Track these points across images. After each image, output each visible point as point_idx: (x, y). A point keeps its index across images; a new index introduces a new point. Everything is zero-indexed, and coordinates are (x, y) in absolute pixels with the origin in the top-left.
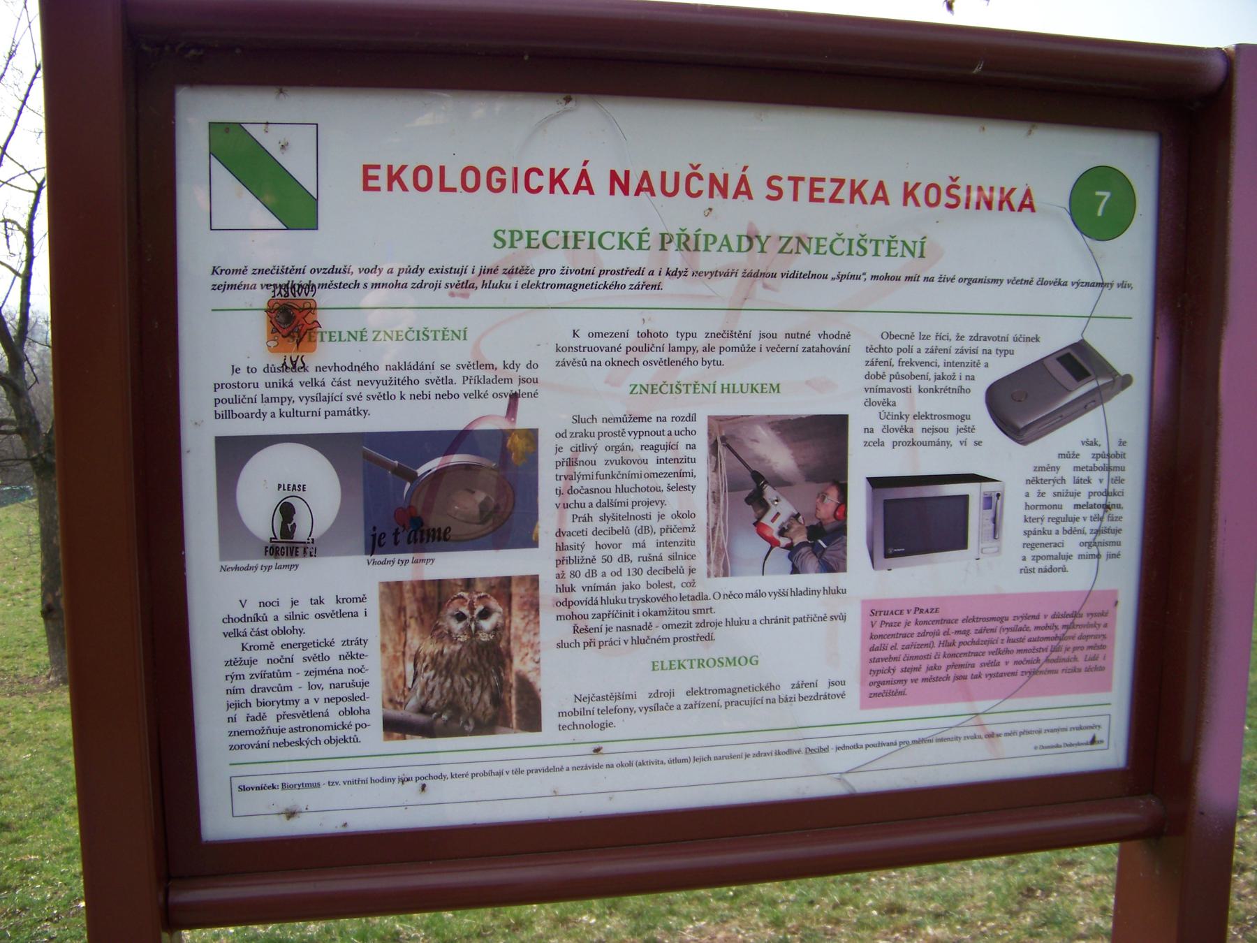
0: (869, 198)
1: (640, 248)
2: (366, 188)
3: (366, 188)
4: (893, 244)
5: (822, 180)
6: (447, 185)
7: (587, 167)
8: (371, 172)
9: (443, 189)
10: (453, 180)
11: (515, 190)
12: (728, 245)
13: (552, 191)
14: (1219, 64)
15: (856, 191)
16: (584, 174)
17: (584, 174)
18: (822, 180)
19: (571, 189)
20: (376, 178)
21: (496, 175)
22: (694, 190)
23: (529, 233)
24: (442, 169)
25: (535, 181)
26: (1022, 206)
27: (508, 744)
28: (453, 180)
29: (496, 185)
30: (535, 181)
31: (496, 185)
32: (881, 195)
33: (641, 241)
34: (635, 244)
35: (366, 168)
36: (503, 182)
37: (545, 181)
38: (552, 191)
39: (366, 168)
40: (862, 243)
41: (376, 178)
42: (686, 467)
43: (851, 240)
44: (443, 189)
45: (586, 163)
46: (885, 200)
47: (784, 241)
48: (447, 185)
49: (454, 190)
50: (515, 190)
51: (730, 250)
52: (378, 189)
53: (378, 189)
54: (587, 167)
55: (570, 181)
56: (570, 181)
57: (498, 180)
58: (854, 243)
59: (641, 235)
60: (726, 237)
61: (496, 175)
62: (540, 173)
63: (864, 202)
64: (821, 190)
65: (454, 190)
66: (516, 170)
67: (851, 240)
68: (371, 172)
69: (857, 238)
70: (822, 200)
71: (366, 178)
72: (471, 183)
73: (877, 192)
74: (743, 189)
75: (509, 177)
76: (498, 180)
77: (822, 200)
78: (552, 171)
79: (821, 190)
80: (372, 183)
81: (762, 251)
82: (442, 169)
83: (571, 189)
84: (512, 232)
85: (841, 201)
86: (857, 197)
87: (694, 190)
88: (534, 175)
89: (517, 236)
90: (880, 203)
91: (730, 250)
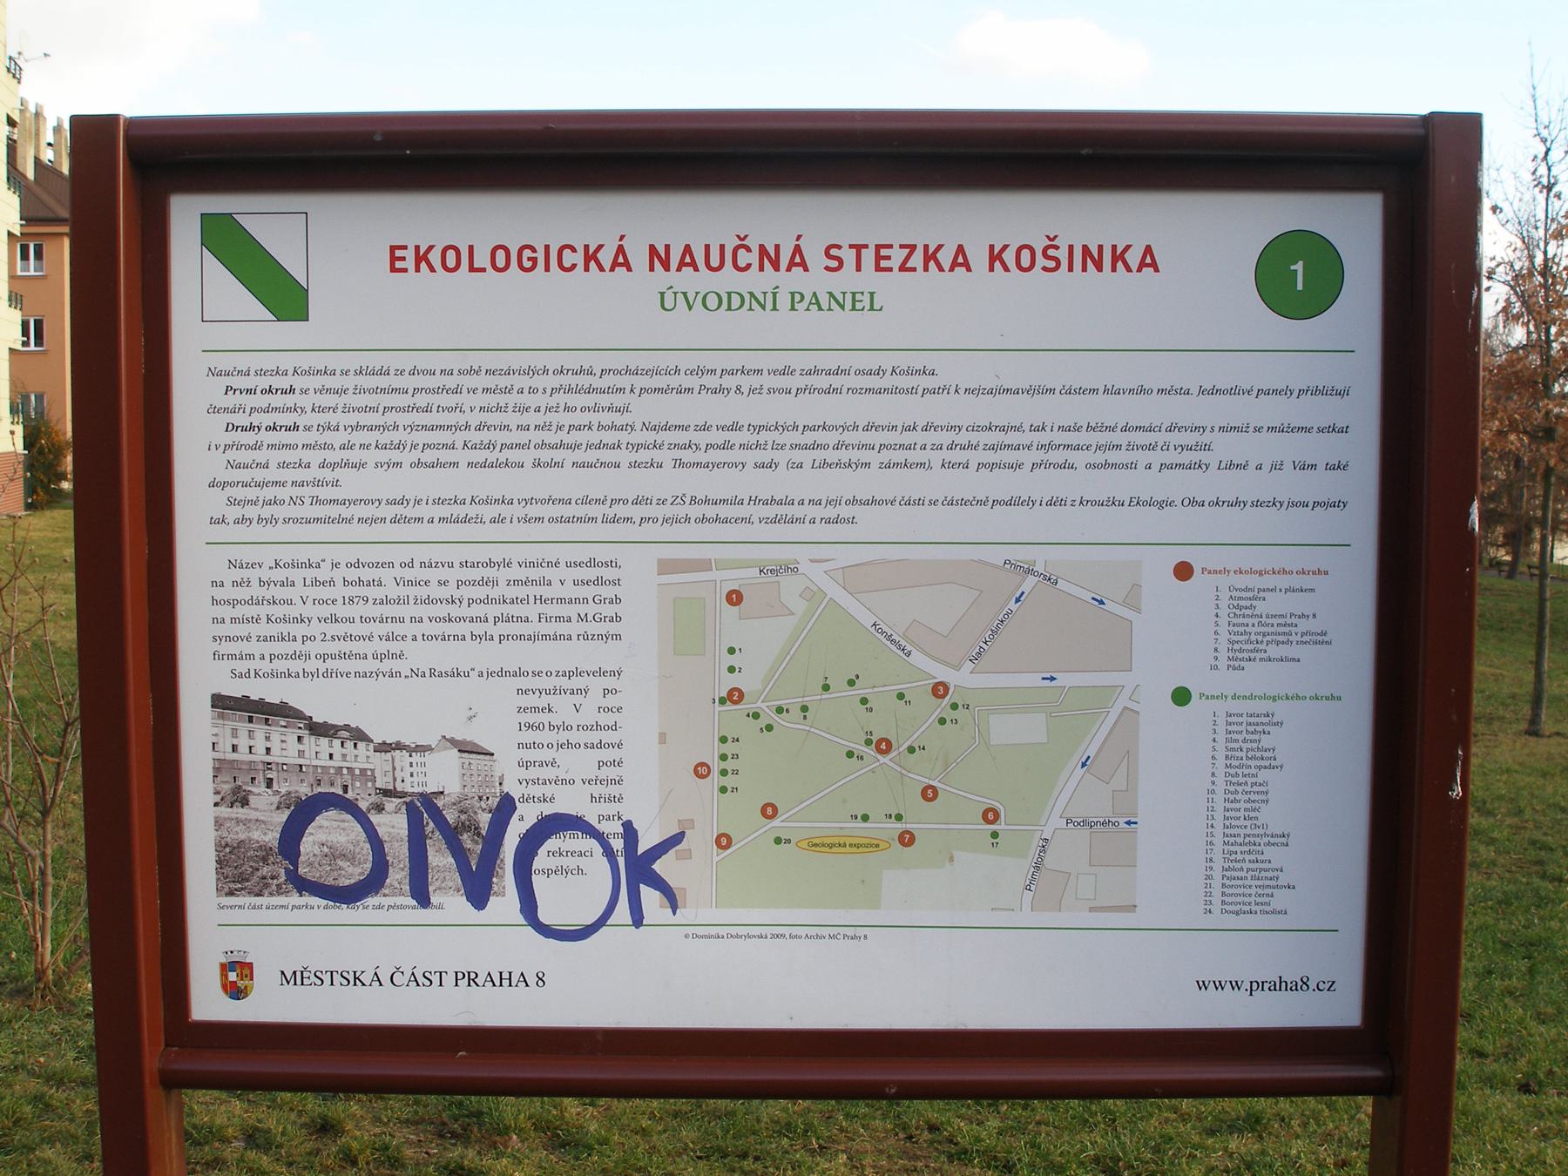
0: (607, 265)
3: (393, 269)
9: (472, 269)
10: (482, 260)
11: (547, 269)
12: (818, 303)
13: (587, 269)
15: (591, 257)
16: (798, 250)
17: (798, 250)
19: (607, 266)
20: (403, 259)
21: (527, 253)
22: (742, 264)
24: (471, 248)
28: (482, 260)
29: (528, 264)
31: (528, 264)
35: (393, 249)
36: (534, 260)
37: (579, 258)
38: (587, 269)
39: (393, 249)
41: (403, 259)
44: (472, 269)
49: (483, 270)
50: (547, 269)
51: (820, 309)
52: (405, 270)
53: (405, 270)
55: (606, 258)
61: (527, 253)
62: (574, 250)
65: (483, 270)
66: (547, 247)
71: (393, 259)
73: (956, 257)
74: (1148, 260)
75: (540, 256)
78: (587, 247)
79: (889, 258)
80: (883, 264)
82: (471, 248)
88: (567, 252)
91: (820, 309)
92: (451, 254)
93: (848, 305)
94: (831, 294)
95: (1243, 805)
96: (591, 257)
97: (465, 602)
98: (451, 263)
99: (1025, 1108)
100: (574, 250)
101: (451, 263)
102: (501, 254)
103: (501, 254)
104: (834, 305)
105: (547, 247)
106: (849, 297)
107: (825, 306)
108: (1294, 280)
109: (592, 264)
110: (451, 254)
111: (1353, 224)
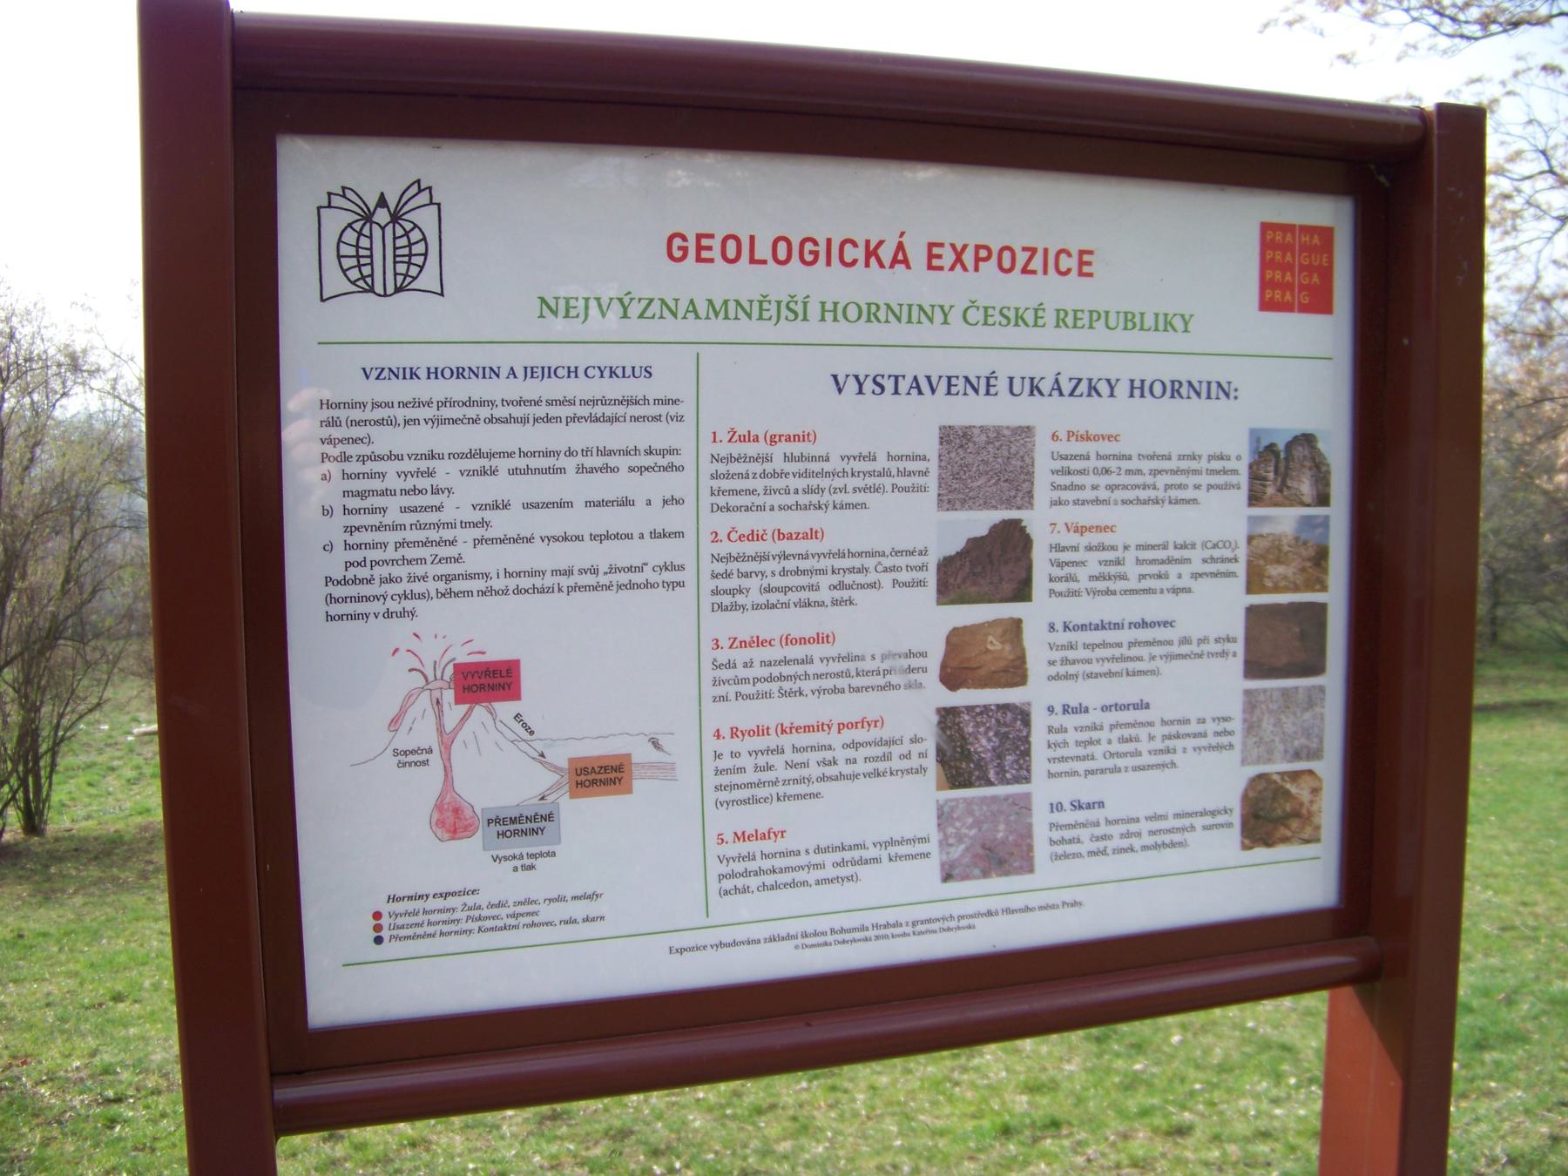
0: (887, 261)
1: (1036, 325)
2: (930, 267)
3: (930, 267)
4: (766, 306)
5: (941, 245)
6: (757, 257)
7: (904, 239)
8: (936, 251)
9: (753, 261)
10: (763, 251)
11: (829, 263)
12: (695, 311)
13: (867, 265)
14: (1416, 121)
15: (871, 253)
16: (900, 247)
17: (900, 247)
18: (941, 245)
19: (887, 262)
20: (709, 248)
21: (809, 246)
22: (848, 259)
23: (1075, 312)
24: (752, 238)
25: (1065, 262)
26: (895, 261)
27: (1028, 877)
28: (763, 251)
29: (809, 258)
30: (1065, 262)
31: (809, 258)
32: (901, 258)
33: (1036, 317)
34: (1030, 321)
35: (931, 245)
36: (816, 254)
37: (859, 253)
38: (867, 265)
39: (931, 245)
40: (792, 305)
41: (709, 248)
42: (1057, 572)
43: (779, 303)
44: (753, 261)
45: (902, 234)
46: (906, 262)
47: (644, 303)
48: (757, 257)
49: (764, 262)
50: (829, 263)
51: (697, 317)
52: (711, 260)
53: (711, 260)
54: (904, 239)
55: (886, 253)
56: (886, 253)
57: (680, 248)
58: (783, 305)
59: (1036, 310)
60: (692, 301)
61: (809, 246)
62: (855, 244)
63: (881, 265)
64: (939, 257)
65: (764, 262)
66: (829, 241)
67: (779, 303)
68: (936, 251)
69: (786, 299)
70: (941, 268)
71: (931, 256)
72: (782, 255)
73: (896, 255)
74: (900, 257)
75: (822, 249)
76: (680, 248)
77: (941, 268)
78: (868, 242)
79: (939, 257)
80: (935, 262)
81: (945, 322)
82: (752, 238)
83: (887, 262)
84: (1091, 312)
85: (1034, 272)
86: (873, 260)
87: (848, 259)
88: (848, 247)
89: (1095, 316)
90: (900, 268)
91: (697, 317)
92: (731, 245)
93: (755, 314)
94: (710, 302)
95: (1071, 737)
96: (871, 253)
97: (835, 728)
98: (731, 254)
99: (1487, 445)
100: (855, 244)
101: (731, 254)
102: (782, 246)
103: (782, 246)
104: (741, 314)
105: (829, 241)
106: (562, 303)
107: (702, 314)
108: (1287, 279)
109: (873, 260)
110: (731, 245)
111: (319, 180)
